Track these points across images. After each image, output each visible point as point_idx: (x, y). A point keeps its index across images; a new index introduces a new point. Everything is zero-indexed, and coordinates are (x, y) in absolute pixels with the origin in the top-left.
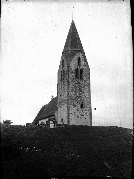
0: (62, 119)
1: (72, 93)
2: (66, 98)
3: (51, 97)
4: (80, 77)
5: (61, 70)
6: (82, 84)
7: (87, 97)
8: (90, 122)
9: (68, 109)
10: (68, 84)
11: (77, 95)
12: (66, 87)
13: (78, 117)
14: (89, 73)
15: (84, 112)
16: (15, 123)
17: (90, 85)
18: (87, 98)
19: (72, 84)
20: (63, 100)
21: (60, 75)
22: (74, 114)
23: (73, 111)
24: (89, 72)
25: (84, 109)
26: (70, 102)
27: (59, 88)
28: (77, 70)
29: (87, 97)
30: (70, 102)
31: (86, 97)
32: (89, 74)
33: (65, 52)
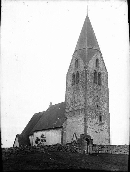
0: (75, 134)
1: (90, 101)
2: (83, 107)
4: (98, 82)
5: (73, 71)
6: (100, 91)
7: (106, 107)
9: (86, 120)
10: (86, 89)
11: (96, 104)
12: (82, 93)
14: (107, 79)
15: (103, 126)
17: (108, 93)
18: (105, 109)
19: (90, 90)
20: (76, 109)
21: (71, 78)
22: (92, 128)
23: (91, 124)
24: (108, 77)
25: (103, 122)
26: (88, 112)
28: (95, 73)
29: (105, 108)
30: (88, 112)
31: (104, 108)
32: (107, 79)
33: (81, 50)
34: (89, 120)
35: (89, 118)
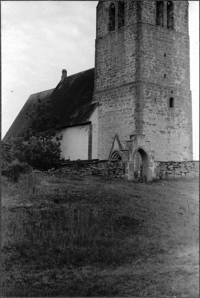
2: (132, 80)
3: (61, 74)
4: (165, 24)
8: (188, 145)
13: (162, 132)
16: (71, 160)
21: (106, 15)
22: (154, 125)
25: (176, 110)
27: (102, 50)
31: (179, 79)
34: (147, 107)
35: (147, 102)
